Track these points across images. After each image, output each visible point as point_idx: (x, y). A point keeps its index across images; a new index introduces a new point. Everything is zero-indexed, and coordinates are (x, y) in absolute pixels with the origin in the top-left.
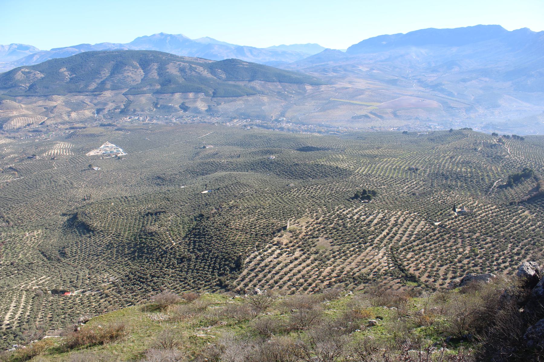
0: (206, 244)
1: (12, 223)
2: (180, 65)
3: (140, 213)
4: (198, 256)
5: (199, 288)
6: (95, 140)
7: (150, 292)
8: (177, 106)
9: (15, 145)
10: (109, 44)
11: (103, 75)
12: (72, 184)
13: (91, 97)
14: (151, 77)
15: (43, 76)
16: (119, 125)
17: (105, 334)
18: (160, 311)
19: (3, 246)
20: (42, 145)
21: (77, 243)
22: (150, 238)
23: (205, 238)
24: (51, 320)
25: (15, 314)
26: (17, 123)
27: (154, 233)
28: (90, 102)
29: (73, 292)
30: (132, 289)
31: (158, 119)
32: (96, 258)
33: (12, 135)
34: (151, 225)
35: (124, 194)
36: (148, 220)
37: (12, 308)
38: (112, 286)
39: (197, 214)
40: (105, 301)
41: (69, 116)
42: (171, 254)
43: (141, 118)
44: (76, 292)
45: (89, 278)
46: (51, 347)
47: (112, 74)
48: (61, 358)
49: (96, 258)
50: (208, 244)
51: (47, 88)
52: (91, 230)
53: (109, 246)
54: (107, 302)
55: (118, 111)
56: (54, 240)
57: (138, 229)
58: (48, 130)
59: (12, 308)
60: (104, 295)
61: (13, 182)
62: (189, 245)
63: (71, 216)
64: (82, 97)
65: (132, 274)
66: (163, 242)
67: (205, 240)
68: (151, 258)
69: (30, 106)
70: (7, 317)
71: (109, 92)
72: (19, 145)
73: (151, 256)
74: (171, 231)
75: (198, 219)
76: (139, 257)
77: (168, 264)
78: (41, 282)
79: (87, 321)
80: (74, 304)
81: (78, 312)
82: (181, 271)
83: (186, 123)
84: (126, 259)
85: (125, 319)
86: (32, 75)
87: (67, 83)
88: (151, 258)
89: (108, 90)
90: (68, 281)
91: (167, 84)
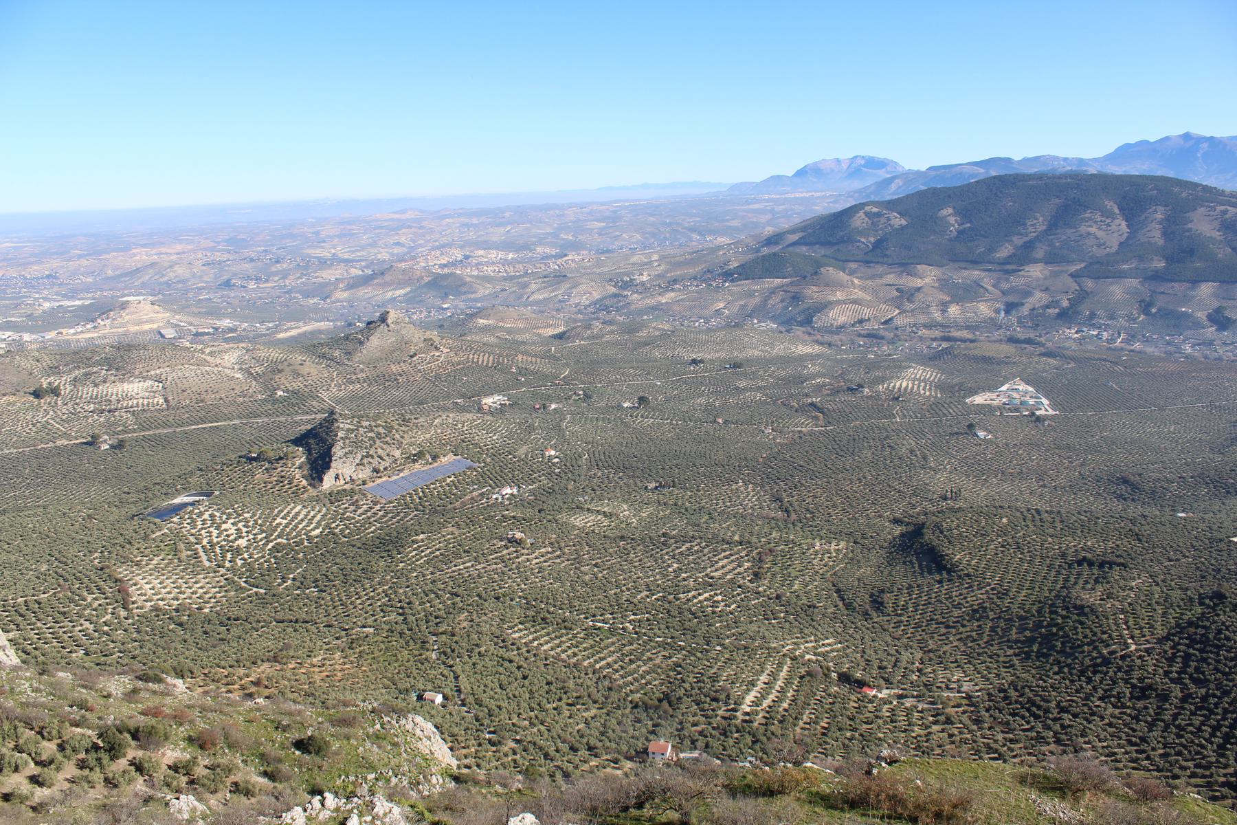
0: (1217, 670)
1: (794, 516)
2: (1225, 212)
3: (1064, 555)
4: (1190, 695)
5: (1176, 777)
6: (991, 371)
7: (1049, 744)
8: (1201, 315)
9: (829, 359)
10: (1054, 158)
11: (1030, 229)
12: (925, 458)
13: (995, 275)
14: (1144, 239)
15: (904, 222)
16: (1049, 345)
17: (925, 803)
18: (1063, 798)
19: (770, 558)
20: (879, 367)
21: (910, 587)
22: (1075, 617)
23: (1218, 655)
24: (824, 734)
25: (763, 697)
26: (838, 316)
27: (1087, 610)
28: (994, 286)
29: (880, 691)
30: (1008, 723)
31: (1147, 341)
32: (943, 630)
33: (827, 338)
34: (1083, 588)
35: (1036, 503)
36: (1079, 575)
37: (760, 685)
38: (964, 702)
39: (1206, 590)
40: (943, 731)
41: (944, 311)
42: (1119, 669)
43: (1105, 334)
44: (886, 691)
45: (919, 670)
46: (814, 789)
47: (1052, 226)
48: (826, 819)
49: (943, 630)
50: (1224, 673)
51: (909, 248)
52: (945, 568)
53: (978, 613)
54: (945, 735)
55: (1053, 311)
56: (866, 570)
57: (1050, 591)
58: (896, 335)
59: (760, 685)
60: (942, 718)
61: (811, 433)
62: (1171, 660)
63: (911, 528)
64: (977, 272)
65: (1016, 690)
66: (1105, 637)
67: (1218, 661)
68: (1068, 666)
69: (869, 282)
70: (750, 698)
71: (1040, 266)
72: (836, 361)
73: (1069, 661)
74: (1133, 615)
75: (1207, 601)
76: (1040, 654)
77: (1105, 691)
78: (822, 649)
79: (896, 761)
80: (877, 717)
81: (881, 735)
82: (1136, 718)
83: (1220, 359)
84: (1010, 652)
85: (976, 786)
86: (883, 220)
87: (950, 240)
88: (1068, 666)
89: (1036, 261)
90: (876, 664)
91: (1183, 259)
